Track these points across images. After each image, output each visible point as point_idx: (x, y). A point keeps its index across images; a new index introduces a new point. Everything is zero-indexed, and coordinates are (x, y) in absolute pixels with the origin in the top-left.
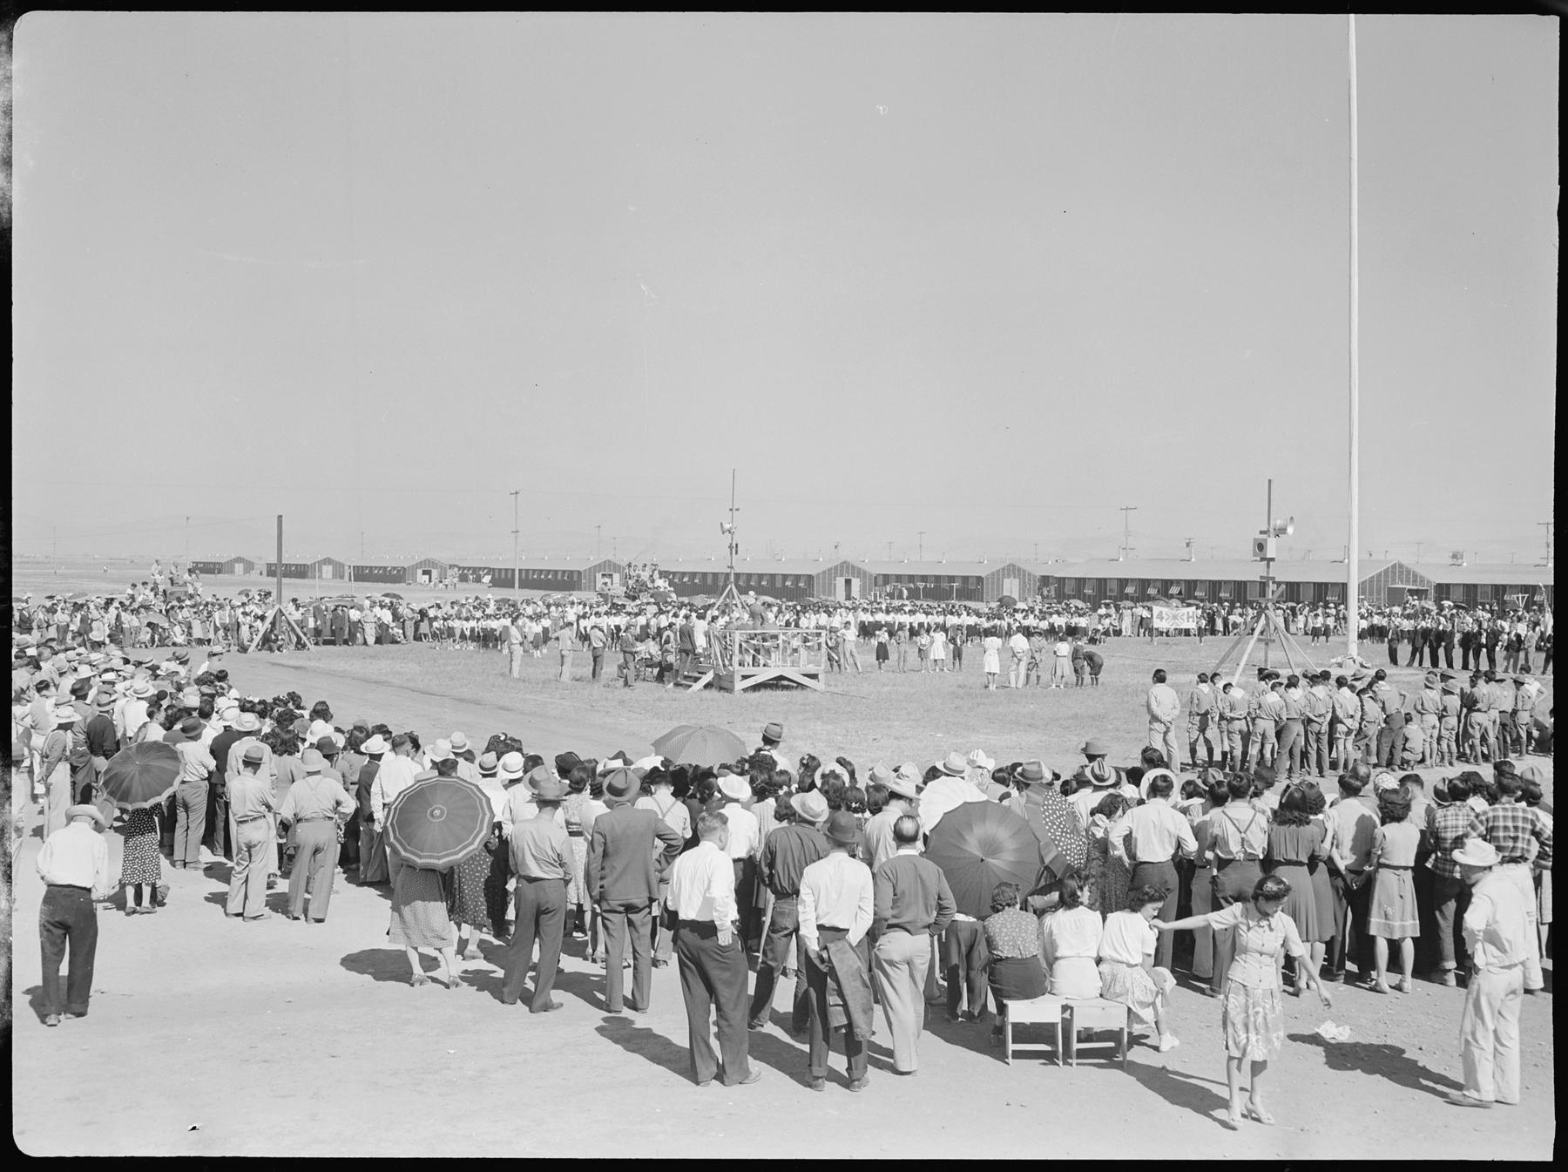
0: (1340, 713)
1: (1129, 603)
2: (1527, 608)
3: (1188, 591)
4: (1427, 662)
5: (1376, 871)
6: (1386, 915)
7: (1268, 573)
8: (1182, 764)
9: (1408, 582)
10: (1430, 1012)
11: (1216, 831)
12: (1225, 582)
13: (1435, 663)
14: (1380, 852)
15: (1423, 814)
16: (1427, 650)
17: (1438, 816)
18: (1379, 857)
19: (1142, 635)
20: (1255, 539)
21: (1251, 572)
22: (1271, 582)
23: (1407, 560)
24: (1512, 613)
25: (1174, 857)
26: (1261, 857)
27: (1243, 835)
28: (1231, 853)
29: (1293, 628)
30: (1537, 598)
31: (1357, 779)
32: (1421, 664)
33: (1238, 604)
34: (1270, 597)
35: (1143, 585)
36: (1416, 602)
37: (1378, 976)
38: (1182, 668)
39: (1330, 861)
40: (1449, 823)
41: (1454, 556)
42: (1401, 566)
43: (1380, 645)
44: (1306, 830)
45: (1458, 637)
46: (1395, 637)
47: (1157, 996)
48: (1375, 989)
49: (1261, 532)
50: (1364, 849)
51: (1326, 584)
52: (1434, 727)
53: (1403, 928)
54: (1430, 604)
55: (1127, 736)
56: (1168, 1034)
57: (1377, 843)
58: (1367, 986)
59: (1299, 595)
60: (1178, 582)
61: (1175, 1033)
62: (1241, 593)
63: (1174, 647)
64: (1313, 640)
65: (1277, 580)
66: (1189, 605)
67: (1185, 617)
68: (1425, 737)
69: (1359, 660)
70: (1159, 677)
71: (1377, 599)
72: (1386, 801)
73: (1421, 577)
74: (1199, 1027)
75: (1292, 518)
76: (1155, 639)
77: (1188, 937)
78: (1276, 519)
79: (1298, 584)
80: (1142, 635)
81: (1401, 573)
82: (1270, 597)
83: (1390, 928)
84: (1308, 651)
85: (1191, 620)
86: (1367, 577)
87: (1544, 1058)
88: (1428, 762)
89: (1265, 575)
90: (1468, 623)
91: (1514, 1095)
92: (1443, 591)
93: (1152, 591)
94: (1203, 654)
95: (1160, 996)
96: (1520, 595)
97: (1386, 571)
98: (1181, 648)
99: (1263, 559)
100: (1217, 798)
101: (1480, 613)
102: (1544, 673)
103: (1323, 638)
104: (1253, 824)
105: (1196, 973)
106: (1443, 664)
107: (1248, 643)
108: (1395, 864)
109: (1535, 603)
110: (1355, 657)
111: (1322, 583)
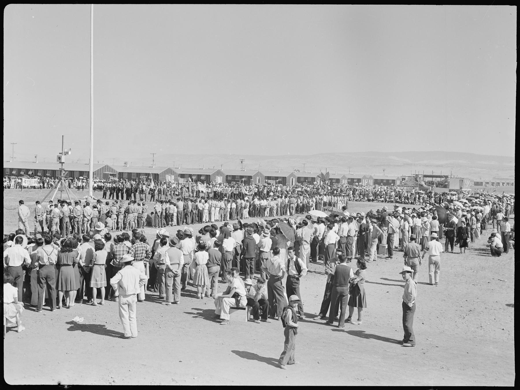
0: (86, 215)
1: (14, 177)
2: (147, 181)
3: (35, 173)
4: (115, 198)
5: (93, 266)
6: (96, 280)
7: (62, 167)
8: (30, 233)
9: (110, 171)
10: (110, 310)
11: (40, 255)
12: (40, 170)
13: (118, 198)
14: (94, 260)
15: (109, 247)
16: (115, 194)
17: (114, 247)
18: (94, 262)
19: (18, 188)
20: (57, 156)
21: (56, 167)
22: (63, 171)
23: (110, 164)
24: (142, 182)
25: (22, 265)
26: (55, 264)
27: (49, 256)
28: (44, 262)
29: (72, 186)
30: (149, 177)
31: (88, 236)
32: (113, 198)
33: (53, 178)
34: (63, 175)
35: (19, 171)
36: (112, 178)
37: (94, 300)
38: (30, 200)
39: (79, 263)
40: (118, 249)
41: (125, 163)
42: (108, 166)
43: (100, 192)
44: (71, 254)
45: (125, 189)
46: (106, 189)
47: (17, 314)
48: (93, 305)
49: (60, 153)
50: (90, 259)
51: (83, 172)
52: (115, 219)
53: (101, 284)
54: (117, 179)
55: (11, 224)
56: (21, 325)
57: (94, 257)
58: (90, 304)
59: (74, 175)
60: (32, 170)
61: (23, 325)
62: (54, 174)
63: (29, 192)
64: (78, 190)
65: (65, 170)
66: (35, 178)
67: (34, 182)
68: (112, 222)
69: (93, 197)
70: (21, 202)
71: (100, 177)
72: (97, 244)
73: (114, 170)
74: (33, 322)
75: (70, 149)
76: (23, 189)
77: (236, 294)
78: (65, 149)
79: (74, 171)
80: (18, 188)
81: (108, 168)
82: (63, 175)
83: (97, 284)
84: (77, 194)
85: (36, 183)
86: (97, 170)
87: (144, 322)
88: (114, 230)
89: (61, 168)
90: (128, 185)
91: (136, 334)
92: (121, 175)
93: (22, 173)
94: (40, 195)
95: (18, 313)
96: (145, 176)
97: (103, 168)
98: (32, 193)
99: (60, 163)
100: (39, 244)
101: (132, 182)
102: (151, 201)
103: (81, 190)
104: (53, 252)
105: (32, 304)
106: (120, 198)
107: (55, 191)
108: (100, 264)
109: (149, 179)
110: (92, 196)
111: (45, 170)
